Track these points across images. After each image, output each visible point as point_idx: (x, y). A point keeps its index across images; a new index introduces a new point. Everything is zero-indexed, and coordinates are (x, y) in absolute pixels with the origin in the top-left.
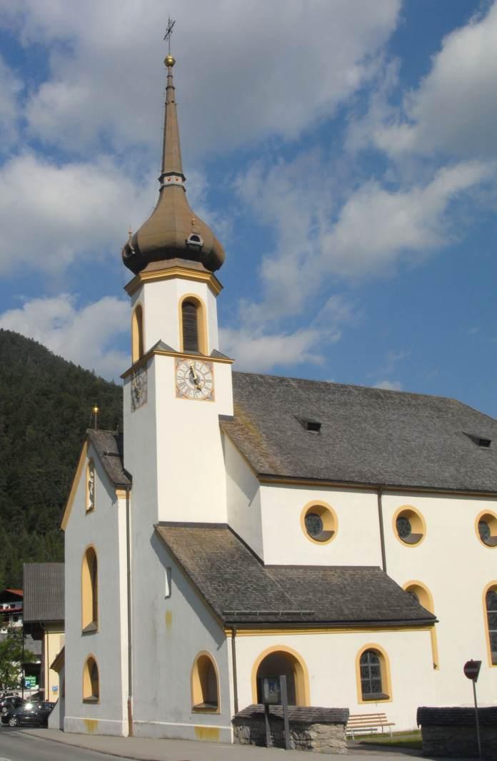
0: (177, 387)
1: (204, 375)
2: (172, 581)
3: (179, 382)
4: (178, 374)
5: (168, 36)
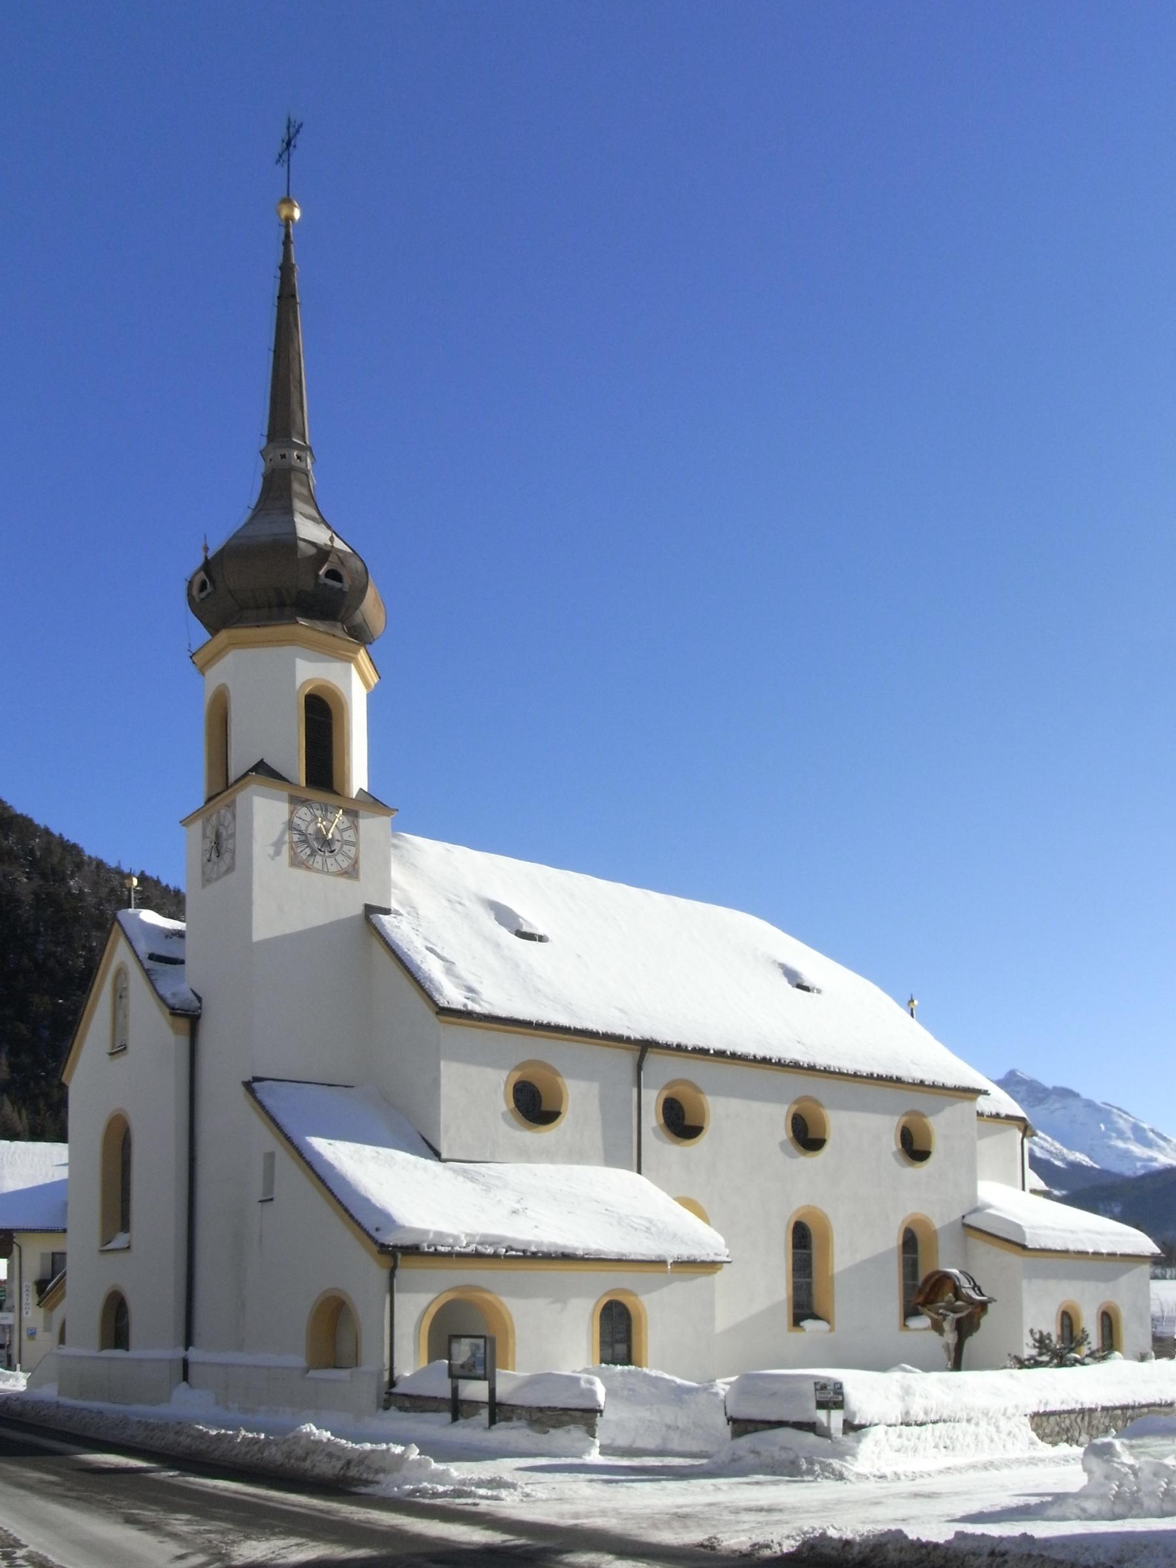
5: (285, 157)
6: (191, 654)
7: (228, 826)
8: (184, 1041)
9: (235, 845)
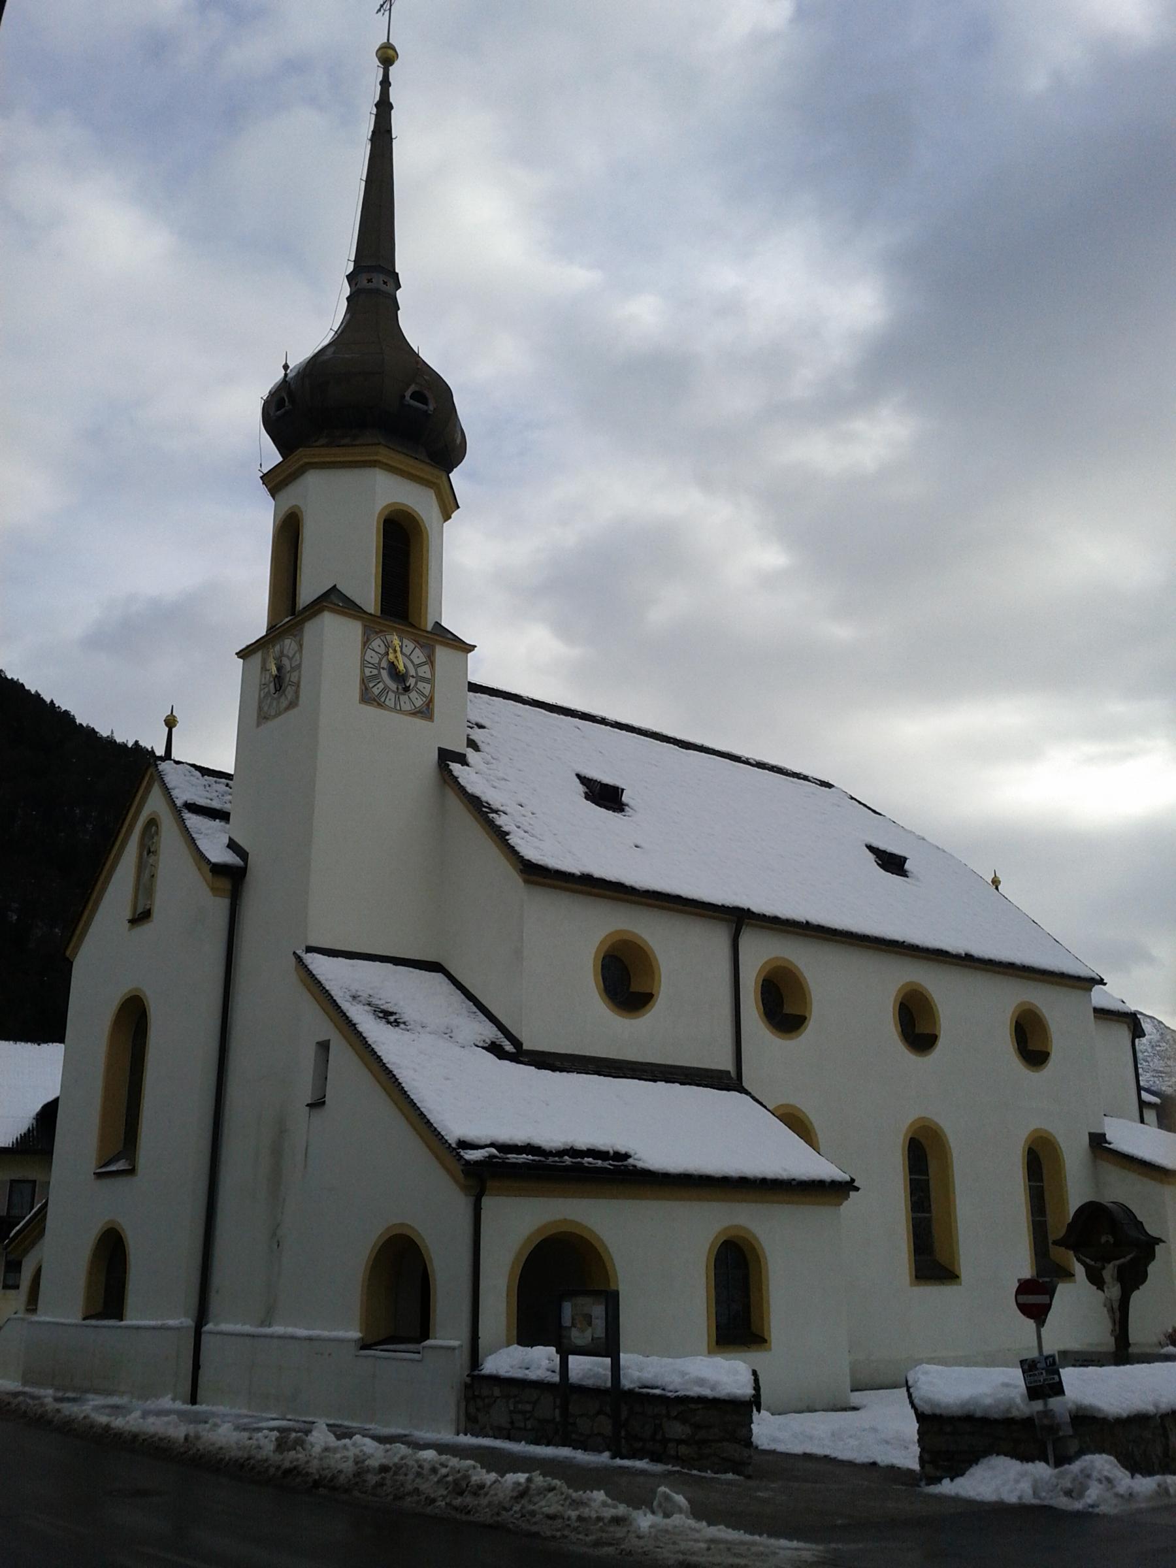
0: (363, 681)
1: (417, 666)
2: (521, 1059)
3: (367, 672)
4: (367, 658)
6: (262, 474)
7: (293, 657)
8: (223, 903)
9: (299, 678)
